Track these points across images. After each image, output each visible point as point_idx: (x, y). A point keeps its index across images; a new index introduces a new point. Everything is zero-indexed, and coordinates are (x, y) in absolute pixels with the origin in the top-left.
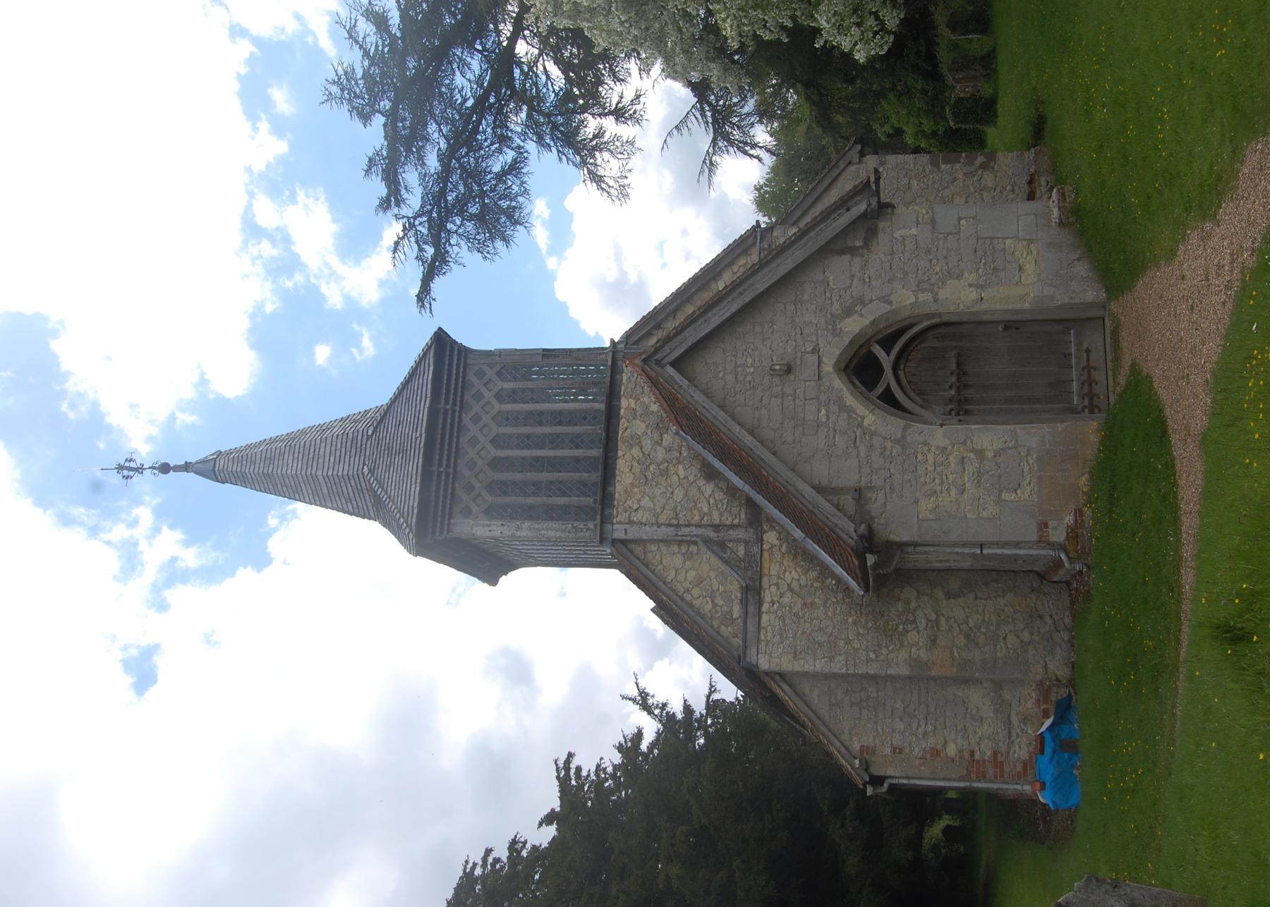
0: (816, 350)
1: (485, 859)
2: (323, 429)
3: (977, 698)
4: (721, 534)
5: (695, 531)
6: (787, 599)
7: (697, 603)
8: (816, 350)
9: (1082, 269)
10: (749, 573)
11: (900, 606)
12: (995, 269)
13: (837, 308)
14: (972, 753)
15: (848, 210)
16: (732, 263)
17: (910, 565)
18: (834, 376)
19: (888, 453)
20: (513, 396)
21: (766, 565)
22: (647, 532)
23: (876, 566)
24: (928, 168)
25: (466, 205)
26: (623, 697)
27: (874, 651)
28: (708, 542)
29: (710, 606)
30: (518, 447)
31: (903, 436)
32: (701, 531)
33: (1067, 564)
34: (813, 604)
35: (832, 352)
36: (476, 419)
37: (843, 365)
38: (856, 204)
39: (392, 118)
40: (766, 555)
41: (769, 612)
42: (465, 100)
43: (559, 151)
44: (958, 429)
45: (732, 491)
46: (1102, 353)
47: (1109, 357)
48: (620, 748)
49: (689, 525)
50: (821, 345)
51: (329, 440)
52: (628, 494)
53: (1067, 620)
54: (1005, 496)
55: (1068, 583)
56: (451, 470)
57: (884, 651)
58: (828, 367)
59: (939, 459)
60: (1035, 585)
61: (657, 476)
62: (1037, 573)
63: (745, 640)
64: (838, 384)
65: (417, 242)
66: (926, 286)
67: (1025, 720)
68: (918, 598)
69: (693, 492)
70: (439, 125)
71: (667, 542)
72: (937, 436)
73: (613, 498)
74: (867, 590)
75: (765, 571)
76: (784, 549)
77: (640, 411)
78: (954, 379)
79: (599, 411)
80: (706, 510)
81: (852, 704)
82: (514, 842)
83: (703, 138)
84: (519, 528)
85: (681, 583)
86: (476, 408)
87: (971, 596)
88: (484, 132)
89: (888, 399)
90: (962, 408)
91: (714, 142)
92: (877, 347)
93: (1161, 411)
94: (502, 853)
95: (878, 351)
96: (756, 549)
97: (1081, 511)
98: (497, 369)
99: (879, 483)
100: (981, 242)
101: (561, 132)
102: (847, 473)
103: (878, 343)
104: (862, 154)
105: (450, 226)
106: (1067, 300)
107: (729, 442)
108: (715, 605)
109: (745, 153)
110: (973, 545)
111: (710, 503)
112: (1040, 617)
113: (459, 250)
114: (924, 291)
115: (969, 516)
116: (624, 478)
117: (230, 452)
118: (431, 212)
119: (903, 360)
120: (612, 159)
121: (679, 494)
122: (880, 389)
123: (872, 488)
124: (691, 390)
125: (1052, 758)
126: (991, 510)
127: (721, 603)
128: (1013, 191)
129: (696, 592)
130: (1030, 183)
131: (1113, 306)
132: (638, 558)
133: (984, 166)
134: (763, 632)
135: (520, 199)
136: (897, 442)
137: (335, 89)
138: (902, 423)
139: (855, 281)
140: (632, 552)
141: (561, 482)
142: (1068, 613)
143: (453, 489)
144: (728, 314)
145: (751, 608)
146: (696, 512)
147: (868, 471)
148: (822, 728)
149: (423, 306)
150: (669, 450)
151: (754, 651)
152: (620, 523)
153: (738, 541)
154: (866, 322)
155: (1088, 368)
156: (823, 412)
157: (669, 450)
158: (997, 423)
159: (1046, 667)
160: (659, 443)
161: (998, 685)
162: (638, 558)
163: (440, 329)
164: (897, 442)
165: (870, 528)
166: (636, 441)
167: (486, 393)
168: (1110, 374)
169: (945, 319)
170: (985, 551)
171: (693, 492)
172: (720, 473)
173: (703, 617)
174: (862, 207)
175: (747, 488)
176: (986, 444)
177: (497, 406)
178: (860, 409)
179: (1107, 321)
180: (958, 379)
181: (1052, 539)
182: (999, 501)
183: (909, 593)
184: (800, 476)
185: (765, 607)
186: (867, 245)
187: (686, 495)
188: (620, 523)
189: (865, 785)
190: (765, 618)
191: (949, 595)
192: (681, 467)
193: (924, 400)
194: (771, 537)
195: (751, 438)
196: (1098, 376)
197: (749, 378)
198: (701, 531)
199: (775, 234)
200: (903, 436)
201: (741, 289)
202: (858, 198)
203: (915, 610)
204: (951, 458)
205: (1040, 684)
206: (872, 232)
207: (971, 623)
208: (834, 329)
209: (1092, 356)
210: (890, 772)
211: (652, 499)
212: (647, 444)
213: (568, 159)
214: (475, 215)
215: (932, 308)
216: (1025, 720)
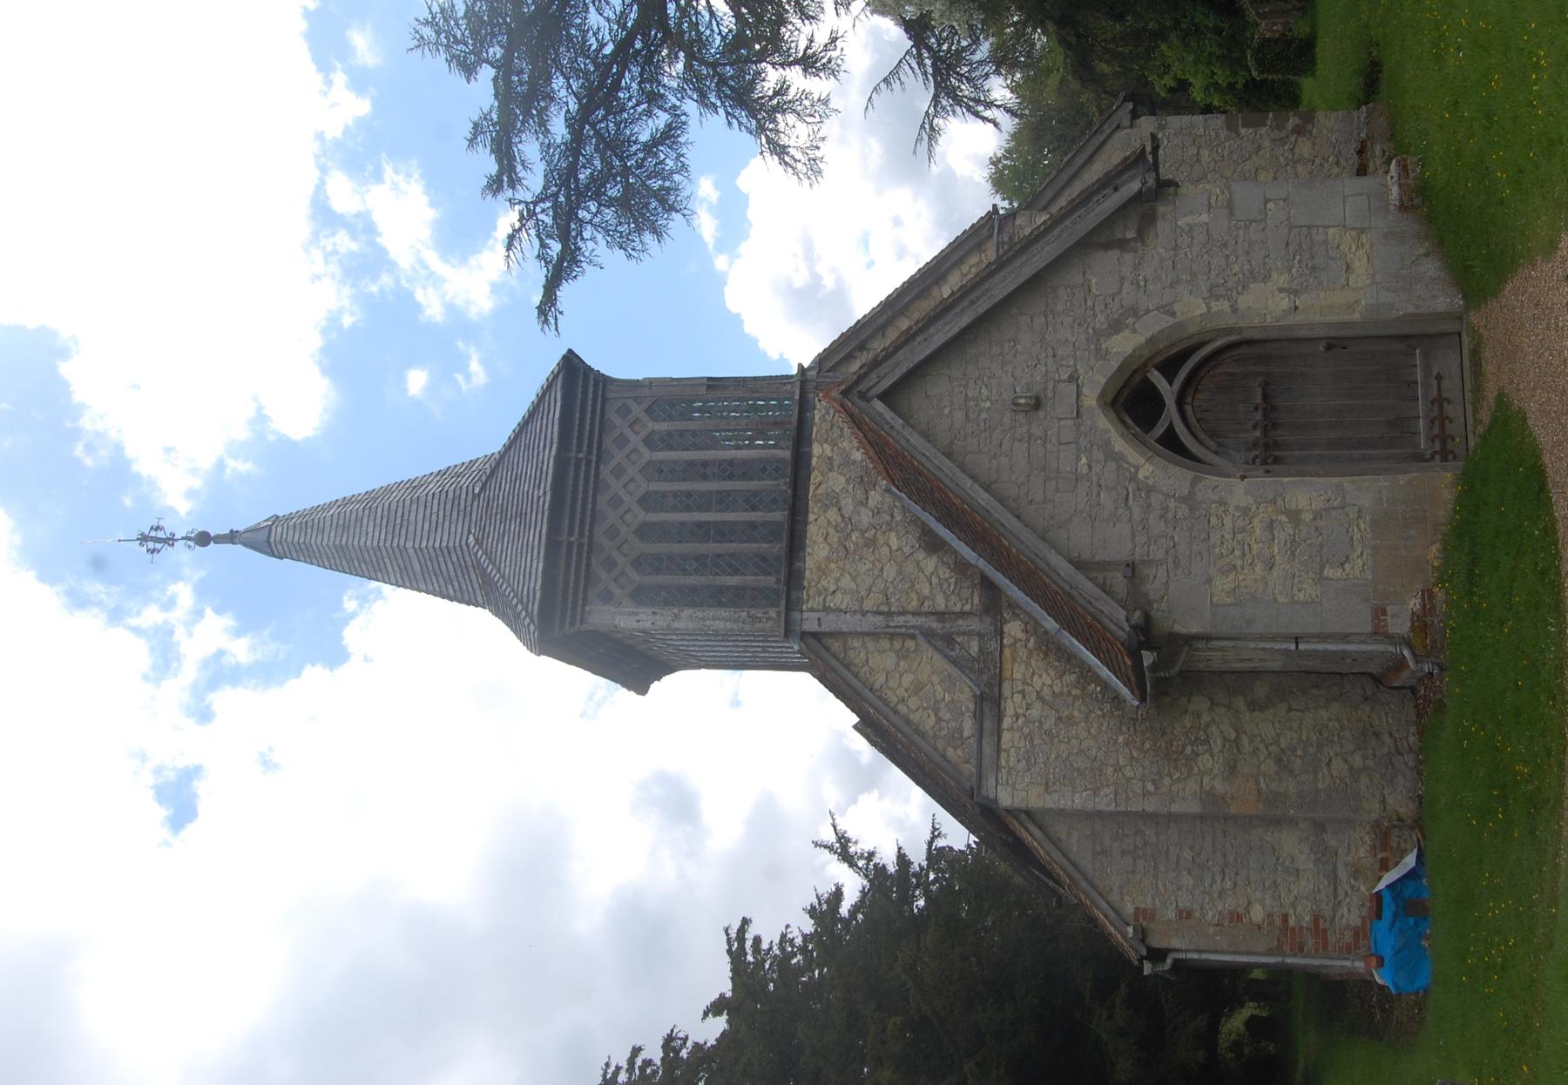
0: (1073, 378)
1: (631, 1061)
2: (413, 485)
3: (1291, 844)
4: (948, 625)
5: (912, 620)
6: (1035, 712)
8: (1073, 378)
9: (1431, 267)
10: (985, 678)
11: (1188, 721)
12: (1314, 268)
13: (1101, 321)
14: (1285, 918)
15: (1116, 189)
16: (960, 261)
17: (1201, 666)
18: (1098, 412)
19: (1170, 515)
21: (1007, 666)
22: (847, 623)
23: (1155, 667)
24: (1223, 134)
25: (604, 185)
26: (816, 844)
27: (1154, 782)
28: (929, 635)
29: (932, 720)
31: (1192, 493)
32: (920, 621)
33: (1411, 664)
36: (618, 472)
37: (1110, 397)
38: (1126, 182)
39: (505, 69)
40: (1007, 653)
41: (1011, 729)
42: (602, 46)
43: (727, 113)
44: (1265, 484)
45: (962, 567)
47: (1468, 386)
49: (903, 613)
50: (1081, 371)
51: (423, 500)
52: (822, 571)
55: (1413, 690)
56: (586, 540)
57: (1167, 781)
58: (1090, 400)
59: (1240, 523)
60: (1369, 692)
61: (861, 548)
62: (1372, 676)
63: (979, 766)
64: (1104, 423)
65: (538, 236)
66: (1221, 291)
68: (1211, 710)
69: (910, 568)
70: (568, 80)
72: (1237, 493)
73: (802, 578)
74: (1143, 699)
75: (1007, 674)
76: (1031, 644)
77: (837, 460)
78: (1258, 416)
80: (926, 592)
81: (1123, 853)
82: (670, 1039)
83: (919, 94)
84: (676, 617)
85: (893, 690)
86: (619, 457)
87: (1283, 707)
88: (628, 88)
89: (1171, 442)
90: (1270, 454)
91: (936, 100)
92: (1156, 373)
93: (1538, 458)
94: (654, 1053)
97: (1431, 595)
99: (1160, 555)
100: (1294, 232)
101: (731, 88)
102: (1116, 542)
103: (1157, 367)
104: (1135, 115)
105: (582, 214)
106: (1411, 309)
107: (958, 502)
108: (939, 720)
109: (977, 114)
110: (1286, 638)
111: (931, 582)
112: (1376, 735)
113: (595, 245)
114: (1217, 298)
115: (1281, 599)
116: (817, 550)
118: (556, 195)
119: (1191, 391)
120: (798, 124)
121: (890, 572)
122: (1160, 430)
123: (1150, 562)
124: (907, 432)
126: (1309, 591)
127: (948, 716)
128: (1337, 163)
129: (913, 702)
130: (1360, 152)
131: (1474, 318)
132: (836, 657)
133: (1298, 131)
134: (1004, 755)
135: (677, 177)
136: (1182, 500)
138: (1190, 475)
139: (1126, 285)
140: (827, 649)
141: (732, 555)
142: (1413, 729)
143: (588, 565)
144: (956, 330)
145: (988, 724)
146: (913, 596)
147: (1144, 539)
148: (1084, 885)
149: (546, 321)
150: (877, 512)
151: (992, 781)
152: (811, 610)
153: (970, 633)
154: (1141, 339)
155: (1440, 401)
156: (1084, 460)
157: (877, 512)
158: (1317, 475)
161: (1320, 827)
162: (836, 657)
163: (570, 351)
164: (1182, 500)
166: (832, 501)
168: (1469, 408)
169: (1247, 335)
170: (1301, 647)
171: (910, 568)
172: (945, 543)
173: (923, 735)
174: (1135, 186)
175: (981, 563)
177: (647, 455)
178: (1133, 455)
179: (1464, 337)
180: (1265, 416)
181: (1393, 630)
182: (1320, 579)
183: (1199, 703)
184: (1053, 546)
186: (1141, 236)
187: (900, 572)
188: (811, 610)
189: (1141, 960)
190: (1006, 736)
191: (1253, 706)
192: (893, 535)
193: (1219, 444)
194: (1014, 629)
195: (986, 496)
197: (984, 415)
198: (920, 621)
199: (1018, 222)
200: (1192, 493)
201: (972, 297)
202: (1130, 173)
204: (1256, 522)
205: (1376, 825)
206: (1149, 220)
208: (1098, 350)
209: (1445, 383)
210: (1175, 943)
211: (854, 578)
212: (848, 504)
213: (740, 123)
214: (616, 199)
215: (1230, 321)
216: (1356, 872)
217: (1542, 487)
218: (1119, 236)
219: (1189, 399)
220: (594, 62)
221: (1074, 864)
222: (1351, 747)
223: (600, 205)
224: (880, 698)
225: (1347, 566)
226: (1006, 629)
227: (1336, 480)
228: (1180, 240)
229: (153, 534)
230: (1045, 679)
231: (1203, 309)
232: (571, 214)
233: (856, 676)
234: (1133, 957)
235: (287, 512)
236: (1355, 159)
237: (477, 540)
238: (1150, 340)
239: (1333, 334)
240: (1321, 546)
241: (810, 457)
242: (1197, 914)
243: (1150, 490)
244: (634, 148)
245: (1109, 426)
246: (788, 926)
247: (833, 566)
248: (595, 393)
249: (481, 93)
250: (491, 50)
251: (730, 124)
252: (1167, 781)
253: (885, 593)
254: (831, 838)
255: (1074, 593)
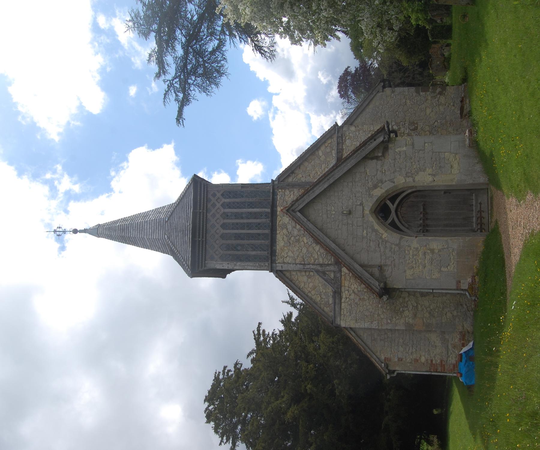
0: (361, 204)
1: (224, 371)
2: (145, 215)
3: (434, 338)
5: (312, 267)
7: (314, 297)
8: (361, 204)
11: (401, 300)
12: (440, 167)
14: (432, 361)
15: (375, 140)
16: (325, 142)
18: (370, 215)
19: (393, 250)
20: (229, 206)
21: (343, 282)
22: (291, 267)
24: (414, 94)
25: (197, 69)
26: (283, 302)
27: (390, 319)
29: (319, 298)
30: (233, 229)
34: (363, 298)
35: (369, 204)
37: (373, 210)
38: (378, 137)
39: (158, 32)
40: (343, 277)
41: (345, 302)
42: (192, 17)
43: (240, 38)
46: (487, 205)
48: (282, 322)
49: (309, 264)
50: (364, 202)
51: (148, 222)
52: (282, 250)
53: (473, 306)
54: (443, 269)
56: (204, 239)
57: (394, 319)
58: (367, 212)
59: (415, 253)
63: (335, 314)
64: (372, 219)
65: (175, 93)
66: (410, 175)
67: (454, 347)
70: (181, 31)
71: (300, 271)
72: (414, 243)
75: (343, 284)
78: (422, 216)
79: (268, 213)
80: (316, 257)
81: (381, 340)
82: (236, 364)
84: (235, 265)
88: (203, 31)
89: (394, 226)
94: (231, 367)
95: (388, 203)
96: (338, 275)
98: (222, 192)
99: (389, 263)
102: (375, 259)
104: (384, 87)
105: (190, 81)
106: (471, 182)
108: (321, 298)
110: (430, 289)
111: (317, 254)
112: (461, 305)
113: (195, 93)
114: (409, 177)
115: (427, 278)
116: (280, 243)
117: (104, 225)
118: (180, 76)
120: (266, 38)
121: (304, 250)
122: (390, 220)
123: (386, 265)
125: (466, 363)
127: (324, 297)
128: (454, 105)
130: (462, 101)
132: (288, 278)
133: (440, 93)
134: (342, 311)
135: (222, 62)
136: (397, 245)
137: (131, 24)
139: (379, 172)
140: (285, 275)
141: (252, 245)
143: (206, 248)
144: (323, 189)
145: (337, 301)
146: (312, 258)
148: (368, 350)
149: (179, 123)
151: (339, 319)
152: (279, 263)
153: (330, 271)
154: (384, 191)
155: (480, 211)
156: (365, 232)
159: (463, 326)
160: (295, 227)
161: (443, 333)
162: (288, 278)
164: (397, 245)
165: (385, 283)
166: (285, 226)
167: (216, 203)
169: (418, 189)
171: (311, 249)
173: (316, 304)
174: (381, 139)
176: (435, 247)
177: (223, 210)
178: (381, 231)
180: (424, 216)
182: (440, 271)
185: (343, 300)
187: (307, 251)
188: (279, 263)
189: (386, 374)
190: (343, 305)
192: (305, 238)
193: (409, 225)
194: (344, 270)
195: (334, 245)
196: (485, 215)
197: (333, 216)
199: (344, 129)
201: (328, 177)
202: (380, 135)
203: (407, 302)
204: (420, 252)
205: (461, 332)
206: (386, 149)
207: (432, 307)
208: (370, 194)
209: (482, 206)
210: (397, 368)
211: (293, 253)
212: (290, 227)
214: (201, 74)
215: (413, 184)
216: (454, 347)
217: (504, 266)
218: (376, 155)
219: (399, 210)
220: (190, 23)
221: (365, 344)
222: (453, 309)
223: (196, 77)
224: (302, 291)
225: (449, 267)
226: (342, 269)
227: (445, 238)
228: (396, 156)
229: (58, 230)
230: (355, 286)
231: (404, 181)
232: (186, 82)
233: (294, 284)
234: (384, 373)
235: (103, 223)
236: (460, 104)
237: (168, 237)
238: (386, 191)
239: (446, 189)
240: (441, 261)
241: (276, 211)
242: (404, 360)
243: (387, 242)
244: (207, 53)
245: (373, 220)
246: (274, 330)
247: (286, 248)
248: (204, 188)
249: (152, 44)
250: (153, 26)
251: (241, 41)
252: (394, 319)
253: (303, 257)
254: (288, 299)
255: (362, 276)
